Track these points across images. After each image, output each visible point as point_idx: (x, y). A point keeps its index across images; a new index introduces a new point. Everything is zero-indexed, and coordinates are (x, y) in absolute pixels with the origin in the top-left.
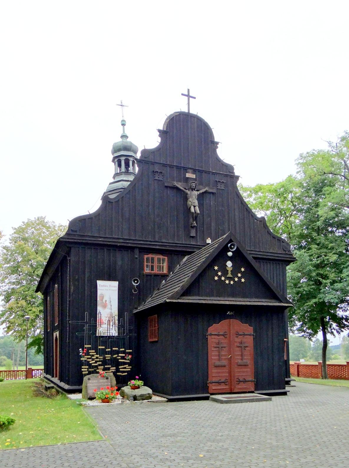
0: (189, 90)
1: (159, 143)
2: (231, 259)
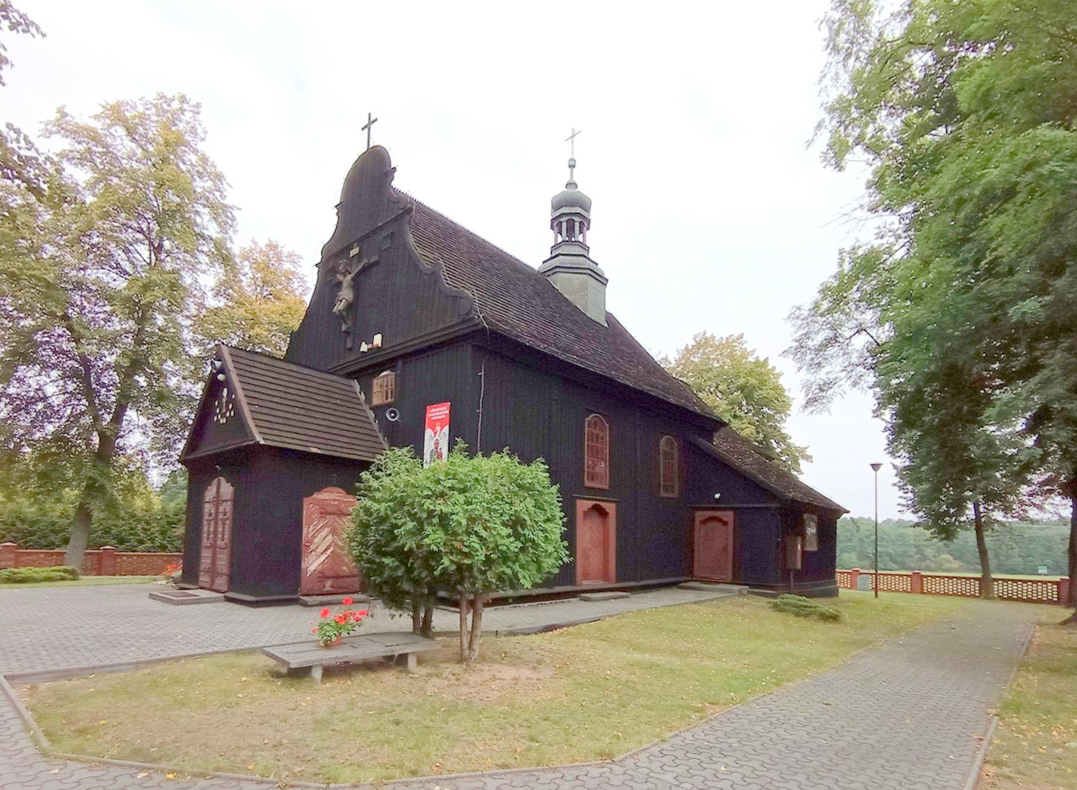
0: (580, 132)
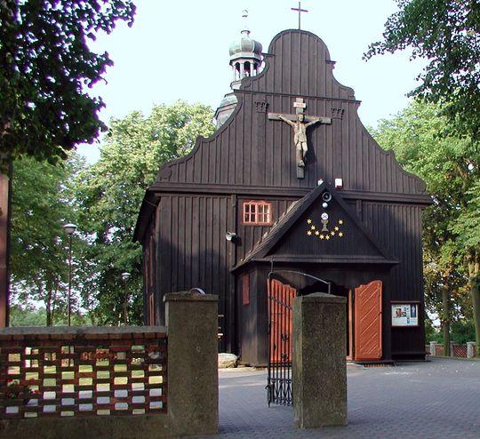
2: (326, 210)
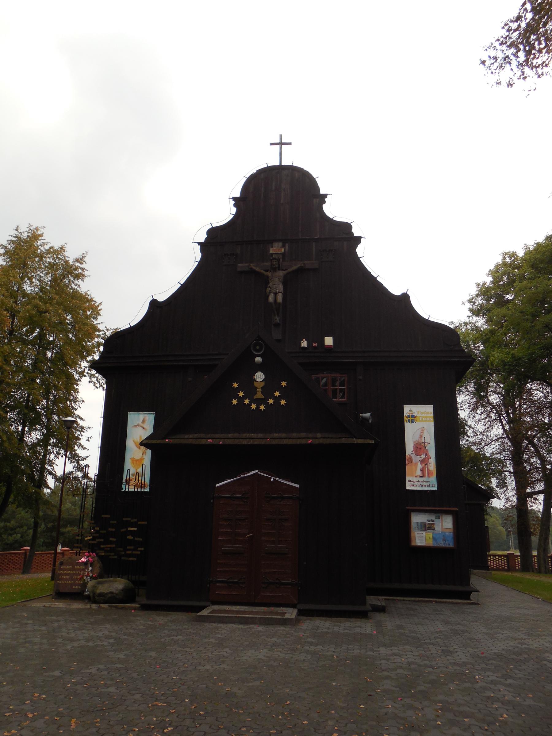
1: (232, 216)
